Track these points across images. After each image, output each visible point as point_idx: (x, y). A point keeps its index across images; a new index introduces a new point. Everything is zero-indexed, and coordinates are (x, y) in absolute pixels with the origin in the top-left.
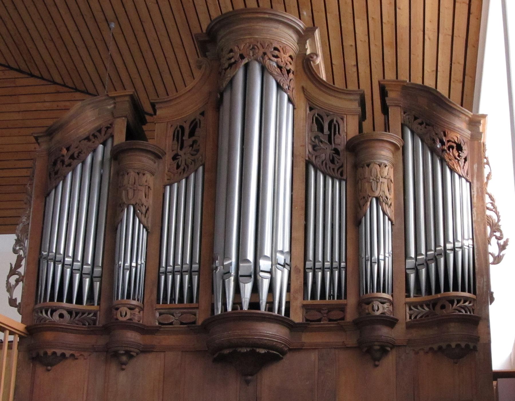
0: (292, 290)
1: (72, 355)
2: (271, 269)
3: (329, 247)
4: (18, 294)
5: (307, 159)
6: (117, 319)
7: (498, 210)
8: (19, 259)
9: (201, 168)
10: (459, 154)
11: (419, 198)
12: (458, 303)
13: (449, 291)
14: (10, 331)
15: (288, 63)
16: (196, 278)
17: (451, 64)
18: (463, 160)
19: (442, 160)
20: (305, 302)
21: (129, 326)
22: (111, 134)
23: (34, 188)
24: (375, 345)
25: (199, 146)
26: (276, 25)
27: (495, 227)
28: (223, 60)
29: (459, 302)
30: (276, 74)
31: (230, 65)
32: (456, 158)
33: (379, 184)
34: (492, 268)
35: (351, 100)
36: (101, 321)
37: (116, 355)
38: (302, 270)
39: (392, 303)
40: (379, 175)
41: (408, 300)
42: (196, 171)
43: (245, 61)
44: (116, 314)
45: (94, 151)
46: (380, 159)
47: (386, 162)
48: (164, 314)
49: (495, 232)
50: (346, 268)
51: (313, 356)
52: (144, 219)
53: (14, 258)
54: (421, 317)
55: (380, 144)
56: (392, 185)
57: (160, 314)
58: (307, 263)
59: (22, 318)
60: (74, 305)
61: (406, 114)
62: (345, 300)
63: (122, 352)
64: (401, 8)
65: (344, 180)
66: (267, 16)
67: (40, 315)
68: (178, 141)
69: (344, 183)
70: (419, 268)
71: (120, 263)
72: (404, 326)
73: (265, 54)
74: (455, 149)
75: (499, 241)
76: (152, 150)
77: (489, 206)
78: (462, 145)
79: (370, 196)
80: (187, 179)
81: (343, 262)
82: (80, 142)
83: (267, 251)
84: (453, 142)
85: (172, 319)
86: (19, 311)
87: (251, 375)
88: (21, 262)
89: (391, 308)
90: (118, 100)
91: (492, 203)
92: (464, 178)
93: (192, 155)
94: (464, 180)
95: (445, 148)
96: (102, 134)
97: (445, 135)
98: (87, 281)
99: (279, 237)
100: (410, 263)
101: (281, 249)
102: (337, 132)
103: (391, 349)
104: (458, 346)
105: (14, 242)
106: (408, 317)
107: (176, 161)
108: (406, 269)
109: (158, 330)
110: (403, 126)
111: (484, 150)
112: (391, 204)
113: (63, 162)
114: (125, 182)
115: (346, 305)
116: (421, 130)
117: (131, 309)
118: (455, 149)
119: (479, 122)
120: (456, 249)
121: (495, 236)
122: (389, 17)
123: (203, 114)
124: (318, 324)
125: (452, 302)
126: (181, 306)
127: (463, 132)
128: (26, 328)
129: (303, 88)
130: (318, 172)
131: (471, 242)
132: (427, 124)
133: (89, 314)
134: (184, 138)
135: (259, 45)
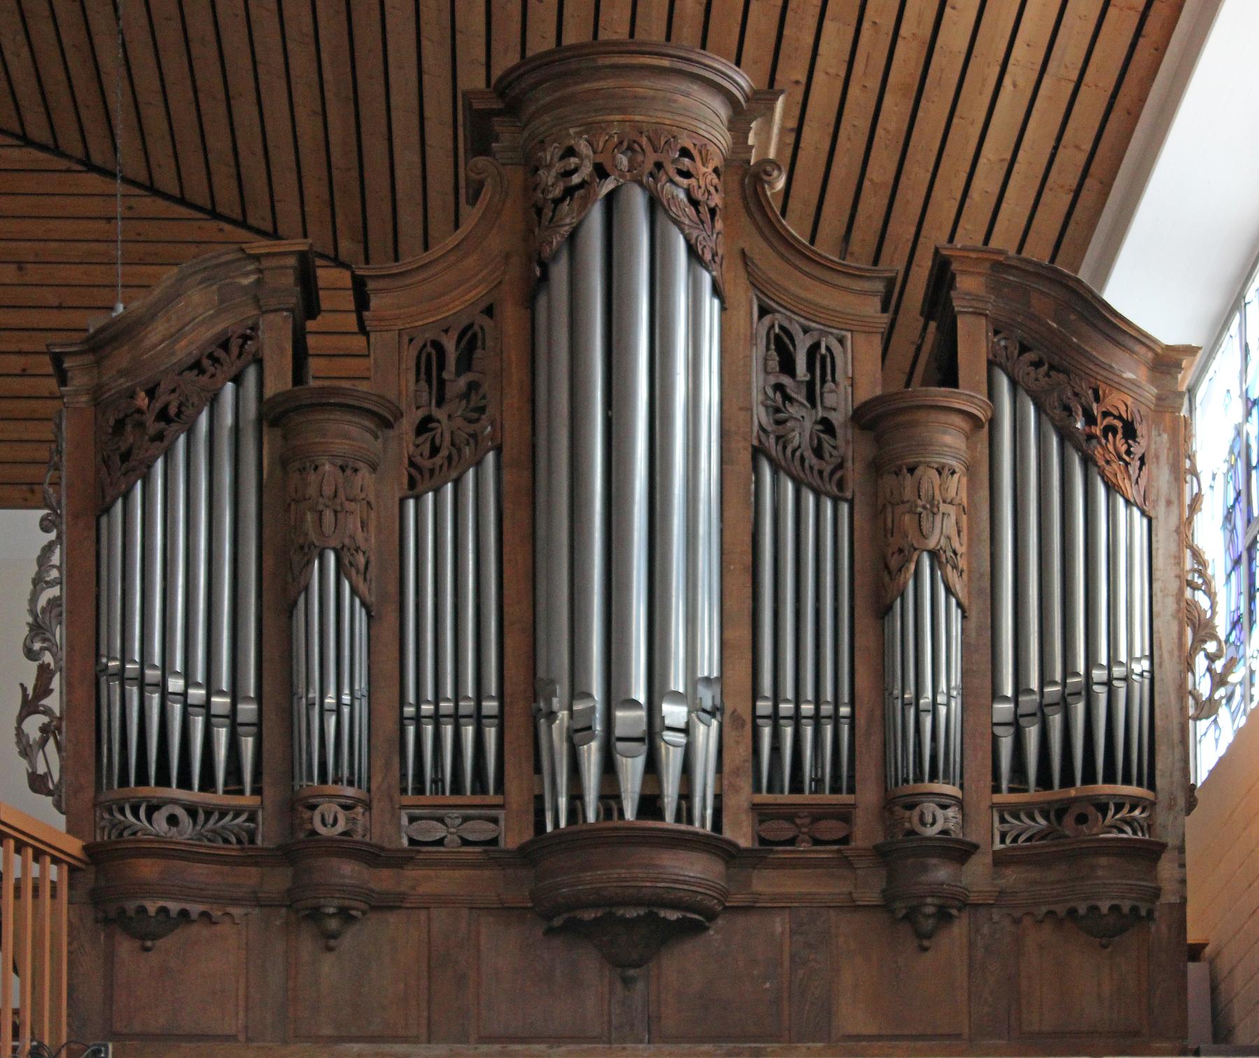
0: (726, 769)
1: (204, 914)
2: (687, 723)
3: (809, 671)
5: (755, 443)
6: (313, 833)
8: (44, 673)
9: (490, 457)
10: (1130, 446)
12: (1116, 813)
13: (1094, 781)
14: (36, 850)
15: (712, 190)
16: (491, 734)
17: (1056, 148)
18: (1138, 463)
19: (1087, 461)
21: (346, 847)
23: (64, 493)
24: (926, 905)
25: (484, 397)
26: (685, 86)
28: (548, 177)
29: (1119, 808)
30: (687, 222)
31: (569, 191)
32: (1121, 458)
33: (938, 518)
35: (865, 293)
36: (267, 834)
37: (315, 915)
38: (748, 718)
39: (960, 803)
40: (938, 497)
41: (997, 798)
42: (478, 464)
43: (609, 185)
44: (311, 819)
45: (214, 401)
47: (954, 463)
51: (779, 925)
52: (362, 587)
53: (29, 673)
54: (1029, 839)
55: (943, 417)
56: (965, 518)
57: (412, 819)
58: (760, 704)
59: (68, 821)
60: (195, 795)
61: (1001, 335)
63: (331, 910)
64: (958, 6)
65: (846, 500)
66: (666, 63)
68: (429, 382)
69: (845, 508)
70: (1022, 721)
71: (310, 695)
72: (988, 859)
73: (659, 166)
74: (1119, 436)
76: (375, 409)
78: (1137, 426)
79: (915, 549)
80: (457, 483)
81: (845, 704)
82: (180, 374)
83: (678, 682)
84: (1115, 417)
85: (438, 831)
86: (58, 805)
87: (638, 966)
88: (50, 683)
90: (266, 263)
91: (1199, 572)
92: (1138, 507)
93: (470, 421)
95: (1097, 430)
96: (230, 353)
97: (1097, 399)
98: (222, 736)
100: (1003, 710)
101: (706, 674)
102: (829, 377)
103: (959, 910)
104: (1115, 909)
105: (26, 631)
106: (997, 839)
107: (428, 435)
109: (412, 858)
110: (991, 364)
111: (1188, 437)
112: (962, 571)
113: (140, 425)
115: (854, 806)
116: (1037, 379)
117: (346, 807)
118: (1119, 436)
119: (1178, 366)
122: (919, 23)
123: (489, 311)
124: (791, 852)
125: (1103, 808)
126: (457, 800)
127: (1139, 391)
128: (84, 848)
129: (743, 253)
130: (782, 475)
131: (1146, 664)
132: (1052, 367)
133: (236, 816)
134: (445, 375)
135: (644, 141)
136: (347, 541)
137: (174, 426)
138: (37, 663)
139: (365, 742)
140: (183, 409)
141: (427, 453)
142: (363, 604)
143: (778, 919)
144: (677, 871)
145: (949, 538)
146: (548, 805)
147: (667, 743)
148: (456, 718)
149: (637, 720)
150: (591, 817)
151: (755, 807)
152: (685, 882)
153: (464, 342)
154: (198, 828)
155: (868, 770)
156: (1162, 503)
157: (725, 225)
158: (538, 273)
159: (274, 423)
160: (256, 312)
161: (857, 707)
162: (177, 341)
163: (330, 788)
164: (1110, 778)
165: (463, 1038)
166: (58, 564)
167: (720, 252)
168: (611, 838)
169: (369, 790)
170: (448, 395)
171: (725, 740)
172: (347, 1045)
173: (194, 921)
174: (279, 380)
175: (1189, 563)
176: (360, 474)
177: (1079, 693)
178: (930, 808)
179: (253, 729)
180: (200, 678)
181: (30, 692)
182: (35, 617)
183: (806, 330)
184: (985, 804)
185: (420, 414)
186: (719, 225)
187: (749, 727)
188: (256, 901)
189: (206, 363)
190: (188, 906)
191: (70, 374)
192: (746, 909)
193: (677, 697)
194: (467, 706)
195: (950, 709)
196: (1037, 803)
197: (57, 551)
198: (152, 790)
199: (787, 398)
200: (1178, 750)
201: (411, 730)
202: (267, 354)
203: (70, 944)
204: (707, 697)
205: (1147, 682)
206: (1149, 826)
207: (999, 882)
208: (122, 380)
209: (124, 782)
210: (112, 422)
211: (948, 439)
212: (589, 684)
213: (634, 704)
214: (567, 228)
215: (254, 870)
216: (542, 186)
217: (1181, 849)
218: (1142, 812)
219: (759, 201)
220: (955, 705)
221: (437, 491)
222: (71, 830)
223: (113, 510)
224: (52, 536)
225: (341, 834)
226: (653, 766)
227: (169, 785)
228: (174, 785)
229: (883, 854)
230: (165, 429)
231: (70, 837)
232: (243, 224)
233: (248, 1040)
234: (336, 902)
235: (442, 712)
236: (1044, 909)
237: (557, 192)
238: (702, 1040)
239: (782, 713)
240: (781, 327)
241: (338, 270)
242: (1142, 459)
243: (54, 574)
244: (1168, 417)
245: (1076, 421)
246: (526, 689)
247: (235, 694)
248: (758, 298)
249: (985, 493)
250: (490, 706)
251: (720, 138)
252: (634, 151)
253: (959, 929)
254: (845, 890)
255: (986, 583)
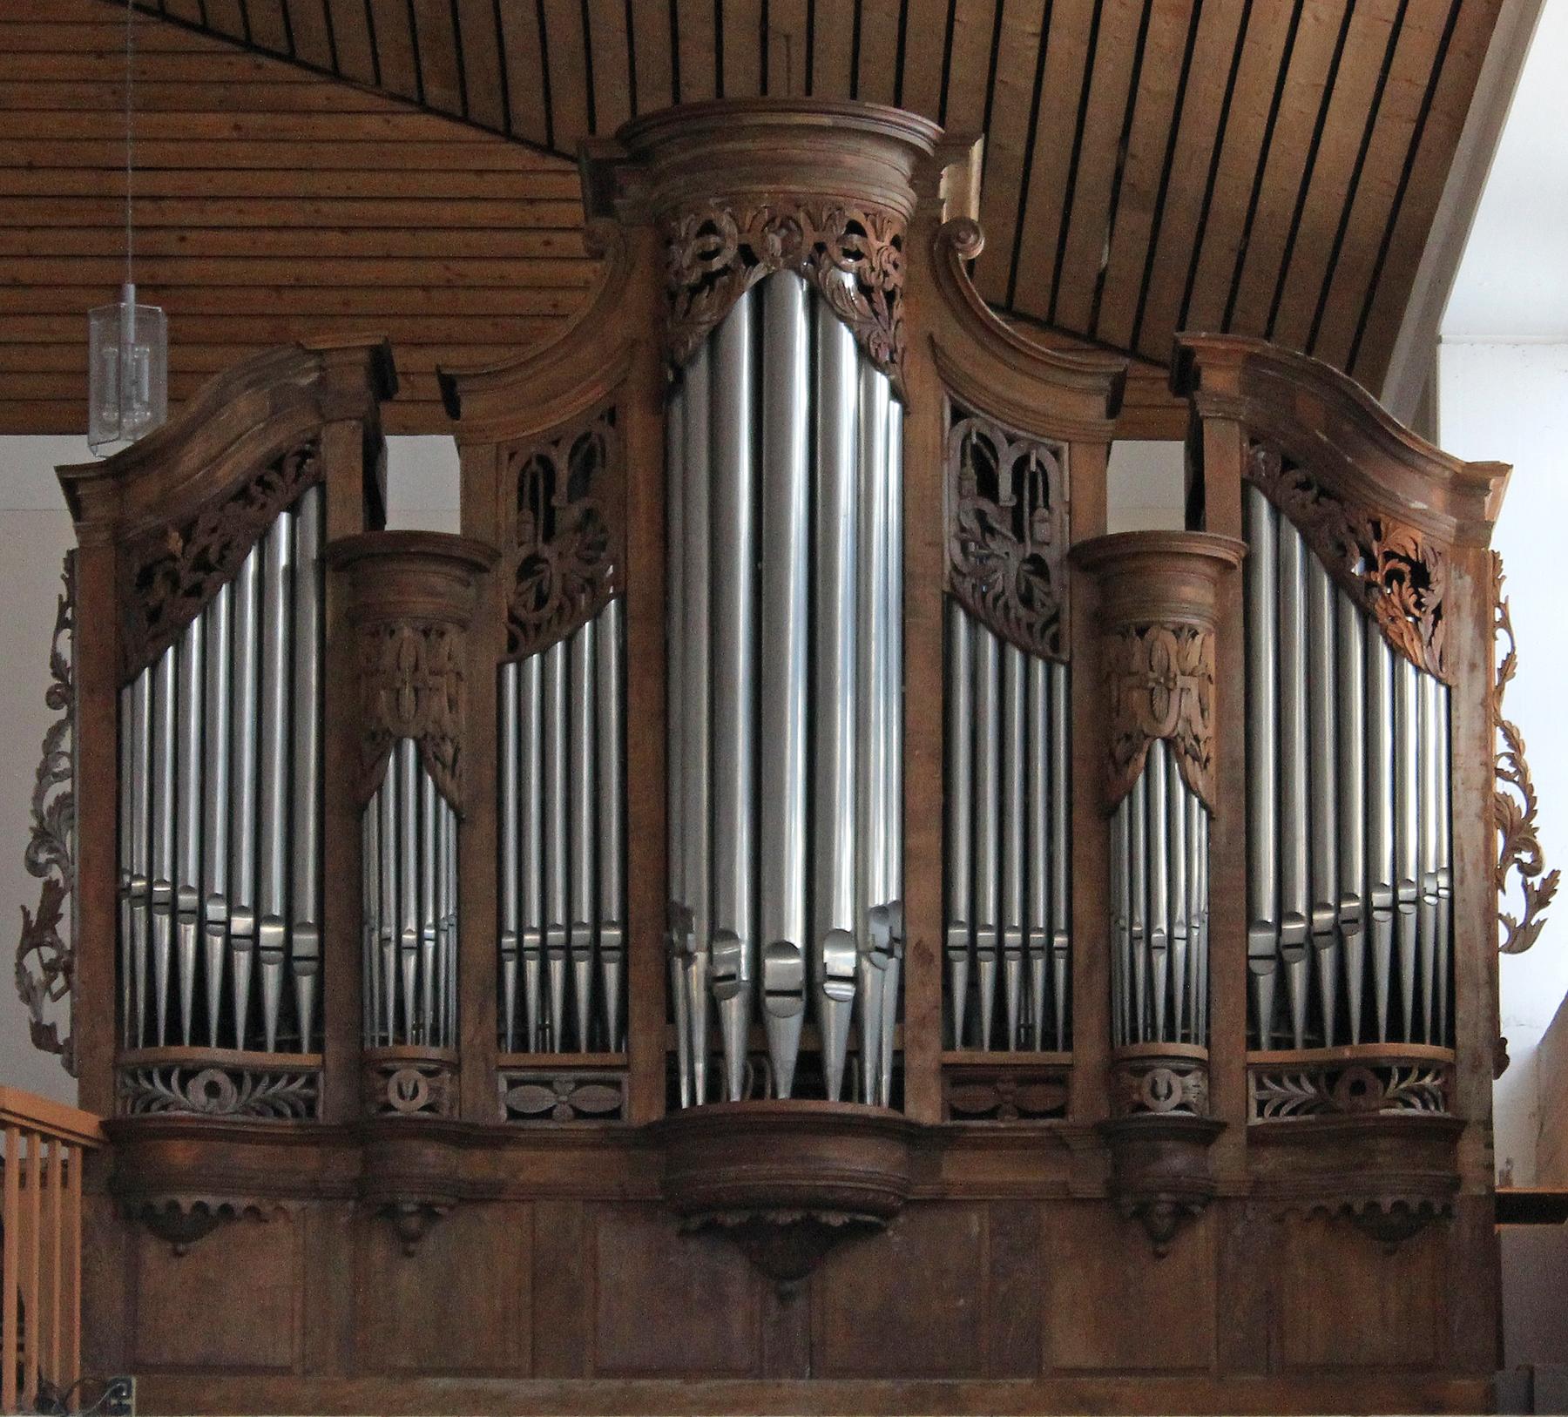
0: (909, 1019)
1: (253, 1211)
2: (858, 969)
3: (1014, 887)
4: (58, 1013)
6: (389, 1107)
7: (1534, 779)
8: (52, 893)
10: (1420, 596)
11: (1291, 678)
12: (1401, 1080)
15: (890, 268)
16: (611, 971)
19: (1367, 617)
20: (950, 1057)
22: (318, 473)
27: (1521, 834)
28: (684, 256)
29: (1405, 1074)
32: (1408, 613)
33: (1175, 696)
34: (1504, 959)
35: (1085, 391)
36: (332, 1100)
40: (1174, 667)
41: (1254, 1057)
42: (597, 615)
43: (758, 273)
45: (264, 538)
46: (1175, 612)
47: (1194, 621)
48: (523, 1082)
49: (1519, 851)
50: (1069, 949)
51: (975, 1223)
52: (450, 785)
53: (32, 893)
54: (1293, 1112)
55: (1182, 564)
56: (1212, 688)
57: (513, 1084)
58: (952, 931)
59: (82, 1089)
60: (239, 1055)
62: (1069, 1054)
63: (410, 1208)
65: (1062, 662)
66: (826, 121)
67: (146, 1085)
68: (535, 510)
69: (1061, 672)
70: (1287, 953)
73: (820, 247)
74: (1406, 584)
75: (1530, 880)
77: (1504, 764)
78: (1430, 568)
79: (1146, 736)
81: (1060, 932)
84: (1402, 559)
85: (544, 1099)
86: (68, 1065)
89: (1204, 1087)
90: (335, 358)
93: (589, 562)
94: (1430, 682)
95: (1378, 578)
97: (1378, 536)
99: (872, 864)
100: (1261, 941)
101: (881, 902)
102: (1041, 501)
103: (1204, 1206)
104: (1399, 1206)
105: (28, 837)
108: (1249, 958)
110: (1246, 485)
111: (1497, 582)
112: (1208, 760)
114: (388, 661)
115: (1070, 1066)
117: (428, 1073)
118: (1406, 584)
119: (1485, 488)
120: (1401, 906)
121: (1518, 861)
125: (1383, 1074)
128: (103, 1125)
129: (931, 338)
131: (1443, 880)
132: (1323, 492)
133: (292, 1080)
135: (802, 217)
136: (431, 728)
137: (215, 575)
138: (43, 879)
139: (453, 978)
140: (226, 553)
141: (531, 603)
142: (451, 805)
143: (975, 1217)
144: (842, 1165)
145: (1189, 721)
146: (684, 1067)
147: (830, 997)
148: (568, 949)
149: (792, 969)
150: (735, 1097)
151: (946, 1068)
152: (851, 1179)
153: (578, 459)
154: (244, 1097)
155: (1089, 1024)
156: (1464, 667)
157: (907, 313)
158: (671, 377)
159: (339, 568)
160: (315, 422)
161: (1076, 936)
162: (219, 466)
163: (409, 1050)
164: (1395, 1035)
165: (575, 1371)
166: (68, 750)
167: (900, 346)
168: (761, 1128)
169: (458, 1050)
170: (558, 527)
171: (908, 982)
172: (429, 1380)
173: (239, 1219)
174: (348, 522)
175: (1501, 745)
176: (447, 639)
177: (1356, 921)
178: (1163, 1075)
179: (312, 965)
180: (246, 901)
181: (34, 917)
182: (41, 820)
183: (1011, 440)
184: (1237, 1065)
185: (523, 552)
186: (898, 312)
187: (938, 961)
188: (314, 1191)
189: (255, 490)
190: (232, 1201)
191: (84, 504)
192: (937, 1202)
193: (842, 939)
194: (582, 935)
195: (1192, 941)
196: (1305, 1064)
197: (68, 733)
198: (186, 1051)
199: (987, 529)
200: (1484, 993)
201: (511, 966)
202: (332, 477)
203: (83, 1246)
204: (881, 934)
205: (1444, 904)
206: (1445, 1096)
207: (1254, 1167)
208: (148, 518)
209: (151, 1039)
210: (137, 569)
211: (1189, 592)
212: (732, 921)
213: (789, 949)
214: (704, 327)
215: (314, 1151)
216: (676, 266)
217: (1488, 1124)
218: (1435, 1078)
219: (950, 271)
220: (1199, 934)
221: (545, 653)
222: (86, 1103)
223: (137, 684)
224: (62, 713)
225: (424, 1109)
226: (813, 1018)
227: (206, 1043)
228: (214, 1042)
229: (1107, 1134)
230: (203, 581)
231: (83, 1113)
232: (290, 58)
233: (306, 1372)
234: (416, 1198)
235: (550, 942)
236: (1314, 1204)
237: (694, 277)
238: (879, 1374)
239: (980, 943)
240: (980, 436)
241: (424, 118)
242: (1438, 613)
243: (64, 763)
244: (1471, 552)
245: (1352, 565)
246: (655, 919)
247: (289, 919)
248: (951, 398)
249: (1239, 654)
250: (612, 935)
251: (900, 199)
252: (789, 229)
253: (1202, 1234)
254: (1061, 1177)
255: (1241, 774)
